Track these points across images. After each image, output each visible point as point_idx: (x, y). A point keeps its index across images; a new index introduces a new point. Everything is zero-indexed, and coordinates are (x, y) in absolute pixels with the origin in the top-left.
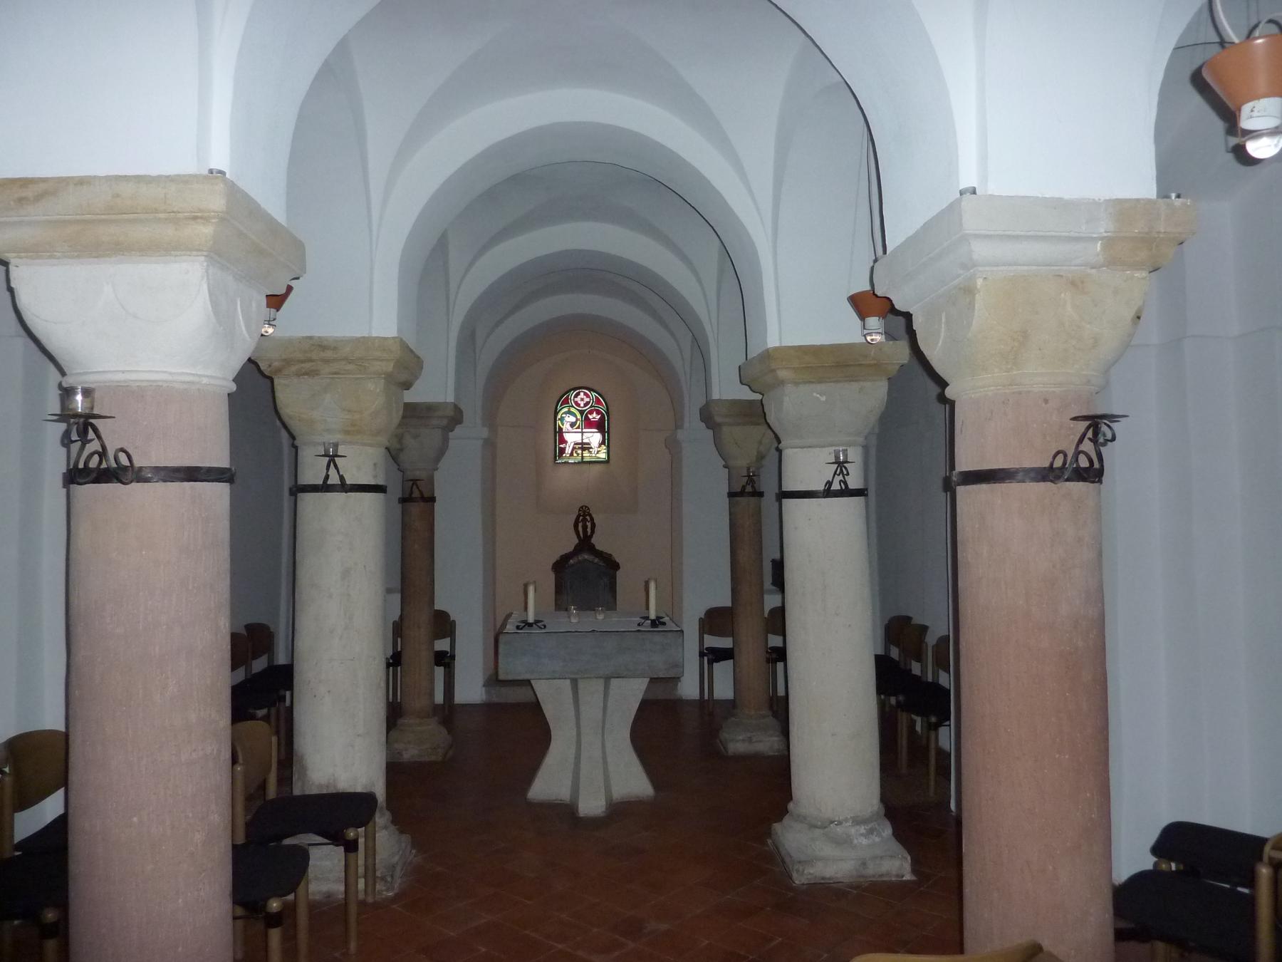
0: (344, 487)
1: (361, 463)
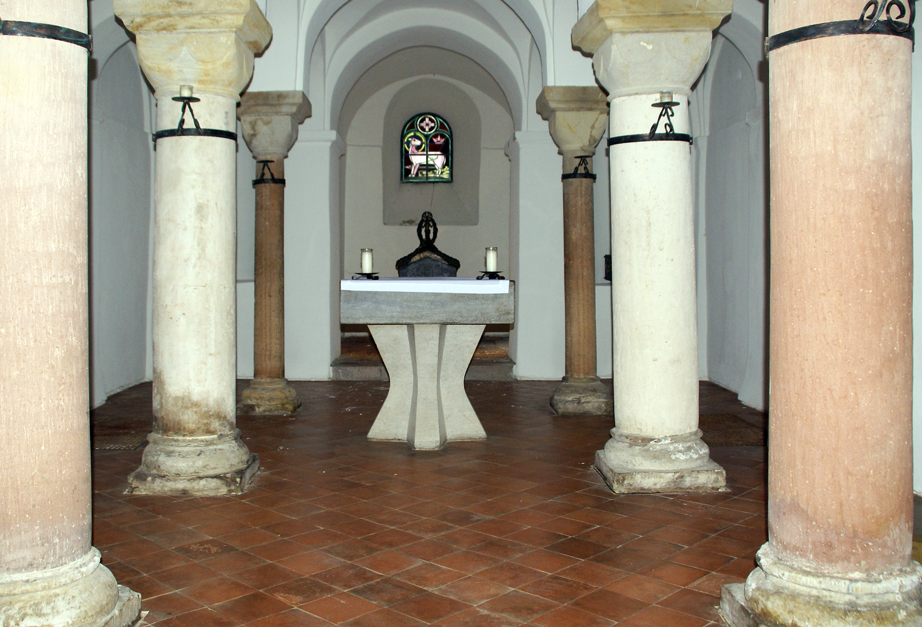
0: (199, 131)
1: (214, 111)
